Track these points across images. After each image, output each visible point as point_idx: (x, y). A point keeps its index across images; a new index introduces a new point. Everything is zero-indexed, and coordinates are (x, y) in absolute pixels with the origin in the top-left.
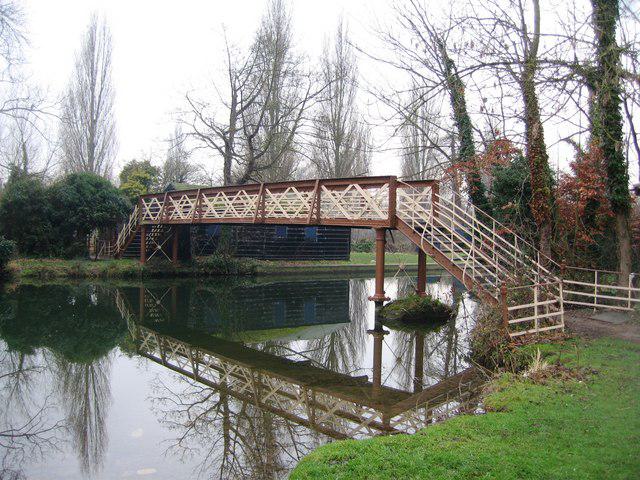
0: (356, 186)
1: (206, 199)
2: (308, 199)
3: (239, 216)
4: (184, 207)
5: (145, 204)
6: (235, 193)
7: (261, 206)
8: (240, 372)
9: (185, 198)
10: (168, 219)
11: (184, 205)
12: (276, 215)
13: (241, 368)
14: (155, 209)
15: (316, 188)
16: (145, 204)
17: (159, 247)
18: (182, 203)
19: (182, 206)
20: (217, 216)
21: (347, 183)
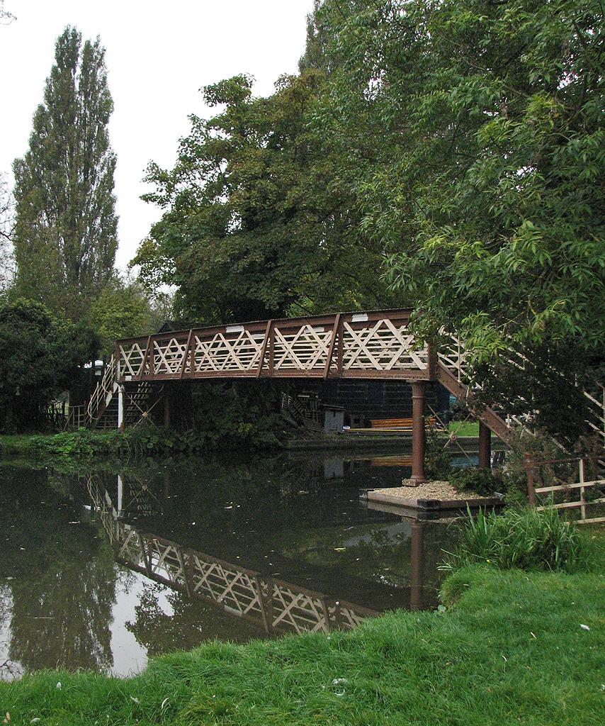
0: (309, 326)
1: (280, 337)
2: (367, 339)
3: (302, 366)
4: (219, 353)
5: (123, 353)
6: (211, 338)
7: (337, 350)
8: (308, 607)
9: (219, 338)
10: (341, 371)
11: (219, 349)
12: (362, 365)
13: (308, 600)
14: (135, 361)
15: (267, 331)
16: (123, 353)
17: (582, 484)
18: (215, 345)
19: (216, 350)
20: (242, 368)
21: (211, 333)
